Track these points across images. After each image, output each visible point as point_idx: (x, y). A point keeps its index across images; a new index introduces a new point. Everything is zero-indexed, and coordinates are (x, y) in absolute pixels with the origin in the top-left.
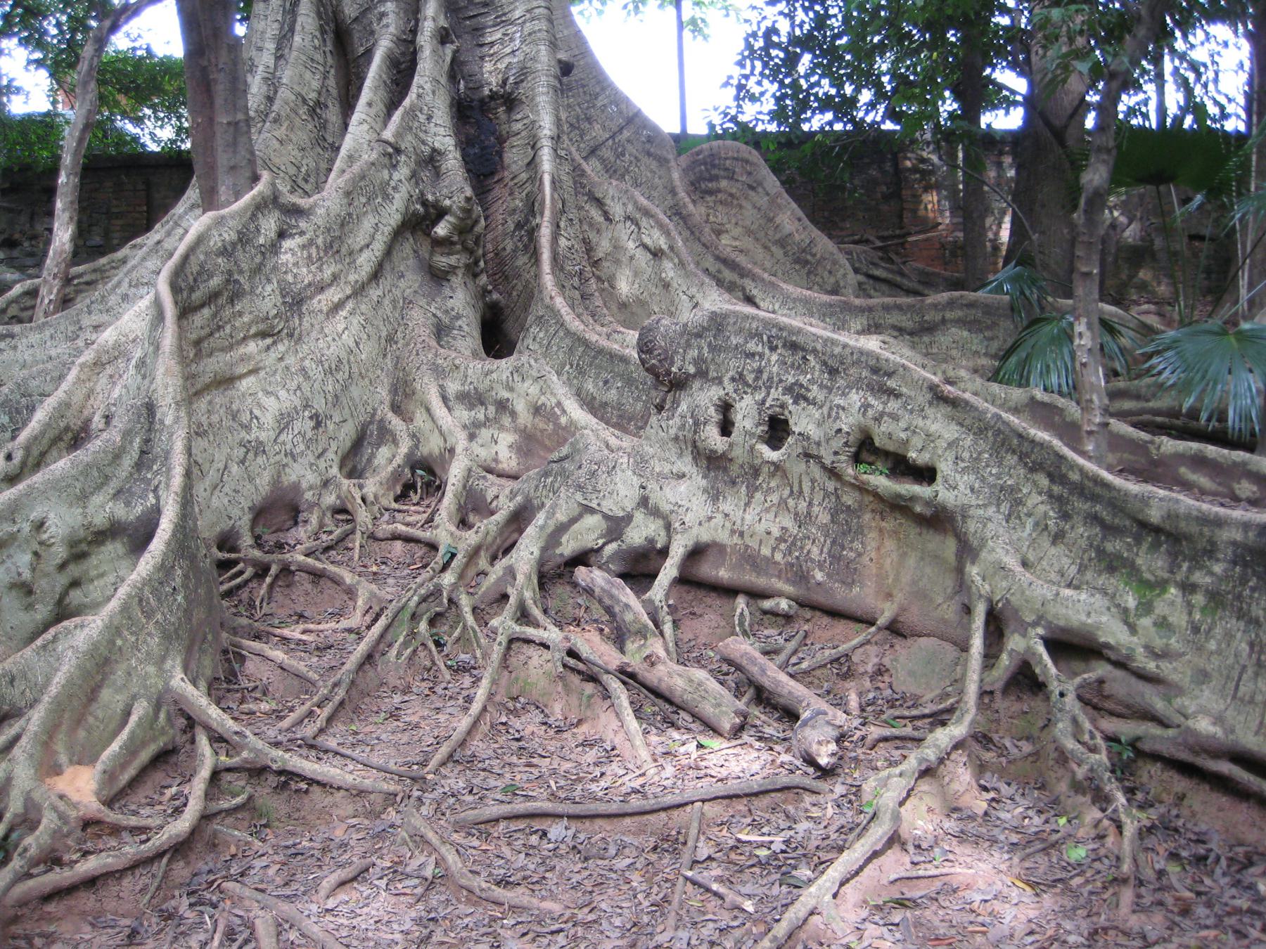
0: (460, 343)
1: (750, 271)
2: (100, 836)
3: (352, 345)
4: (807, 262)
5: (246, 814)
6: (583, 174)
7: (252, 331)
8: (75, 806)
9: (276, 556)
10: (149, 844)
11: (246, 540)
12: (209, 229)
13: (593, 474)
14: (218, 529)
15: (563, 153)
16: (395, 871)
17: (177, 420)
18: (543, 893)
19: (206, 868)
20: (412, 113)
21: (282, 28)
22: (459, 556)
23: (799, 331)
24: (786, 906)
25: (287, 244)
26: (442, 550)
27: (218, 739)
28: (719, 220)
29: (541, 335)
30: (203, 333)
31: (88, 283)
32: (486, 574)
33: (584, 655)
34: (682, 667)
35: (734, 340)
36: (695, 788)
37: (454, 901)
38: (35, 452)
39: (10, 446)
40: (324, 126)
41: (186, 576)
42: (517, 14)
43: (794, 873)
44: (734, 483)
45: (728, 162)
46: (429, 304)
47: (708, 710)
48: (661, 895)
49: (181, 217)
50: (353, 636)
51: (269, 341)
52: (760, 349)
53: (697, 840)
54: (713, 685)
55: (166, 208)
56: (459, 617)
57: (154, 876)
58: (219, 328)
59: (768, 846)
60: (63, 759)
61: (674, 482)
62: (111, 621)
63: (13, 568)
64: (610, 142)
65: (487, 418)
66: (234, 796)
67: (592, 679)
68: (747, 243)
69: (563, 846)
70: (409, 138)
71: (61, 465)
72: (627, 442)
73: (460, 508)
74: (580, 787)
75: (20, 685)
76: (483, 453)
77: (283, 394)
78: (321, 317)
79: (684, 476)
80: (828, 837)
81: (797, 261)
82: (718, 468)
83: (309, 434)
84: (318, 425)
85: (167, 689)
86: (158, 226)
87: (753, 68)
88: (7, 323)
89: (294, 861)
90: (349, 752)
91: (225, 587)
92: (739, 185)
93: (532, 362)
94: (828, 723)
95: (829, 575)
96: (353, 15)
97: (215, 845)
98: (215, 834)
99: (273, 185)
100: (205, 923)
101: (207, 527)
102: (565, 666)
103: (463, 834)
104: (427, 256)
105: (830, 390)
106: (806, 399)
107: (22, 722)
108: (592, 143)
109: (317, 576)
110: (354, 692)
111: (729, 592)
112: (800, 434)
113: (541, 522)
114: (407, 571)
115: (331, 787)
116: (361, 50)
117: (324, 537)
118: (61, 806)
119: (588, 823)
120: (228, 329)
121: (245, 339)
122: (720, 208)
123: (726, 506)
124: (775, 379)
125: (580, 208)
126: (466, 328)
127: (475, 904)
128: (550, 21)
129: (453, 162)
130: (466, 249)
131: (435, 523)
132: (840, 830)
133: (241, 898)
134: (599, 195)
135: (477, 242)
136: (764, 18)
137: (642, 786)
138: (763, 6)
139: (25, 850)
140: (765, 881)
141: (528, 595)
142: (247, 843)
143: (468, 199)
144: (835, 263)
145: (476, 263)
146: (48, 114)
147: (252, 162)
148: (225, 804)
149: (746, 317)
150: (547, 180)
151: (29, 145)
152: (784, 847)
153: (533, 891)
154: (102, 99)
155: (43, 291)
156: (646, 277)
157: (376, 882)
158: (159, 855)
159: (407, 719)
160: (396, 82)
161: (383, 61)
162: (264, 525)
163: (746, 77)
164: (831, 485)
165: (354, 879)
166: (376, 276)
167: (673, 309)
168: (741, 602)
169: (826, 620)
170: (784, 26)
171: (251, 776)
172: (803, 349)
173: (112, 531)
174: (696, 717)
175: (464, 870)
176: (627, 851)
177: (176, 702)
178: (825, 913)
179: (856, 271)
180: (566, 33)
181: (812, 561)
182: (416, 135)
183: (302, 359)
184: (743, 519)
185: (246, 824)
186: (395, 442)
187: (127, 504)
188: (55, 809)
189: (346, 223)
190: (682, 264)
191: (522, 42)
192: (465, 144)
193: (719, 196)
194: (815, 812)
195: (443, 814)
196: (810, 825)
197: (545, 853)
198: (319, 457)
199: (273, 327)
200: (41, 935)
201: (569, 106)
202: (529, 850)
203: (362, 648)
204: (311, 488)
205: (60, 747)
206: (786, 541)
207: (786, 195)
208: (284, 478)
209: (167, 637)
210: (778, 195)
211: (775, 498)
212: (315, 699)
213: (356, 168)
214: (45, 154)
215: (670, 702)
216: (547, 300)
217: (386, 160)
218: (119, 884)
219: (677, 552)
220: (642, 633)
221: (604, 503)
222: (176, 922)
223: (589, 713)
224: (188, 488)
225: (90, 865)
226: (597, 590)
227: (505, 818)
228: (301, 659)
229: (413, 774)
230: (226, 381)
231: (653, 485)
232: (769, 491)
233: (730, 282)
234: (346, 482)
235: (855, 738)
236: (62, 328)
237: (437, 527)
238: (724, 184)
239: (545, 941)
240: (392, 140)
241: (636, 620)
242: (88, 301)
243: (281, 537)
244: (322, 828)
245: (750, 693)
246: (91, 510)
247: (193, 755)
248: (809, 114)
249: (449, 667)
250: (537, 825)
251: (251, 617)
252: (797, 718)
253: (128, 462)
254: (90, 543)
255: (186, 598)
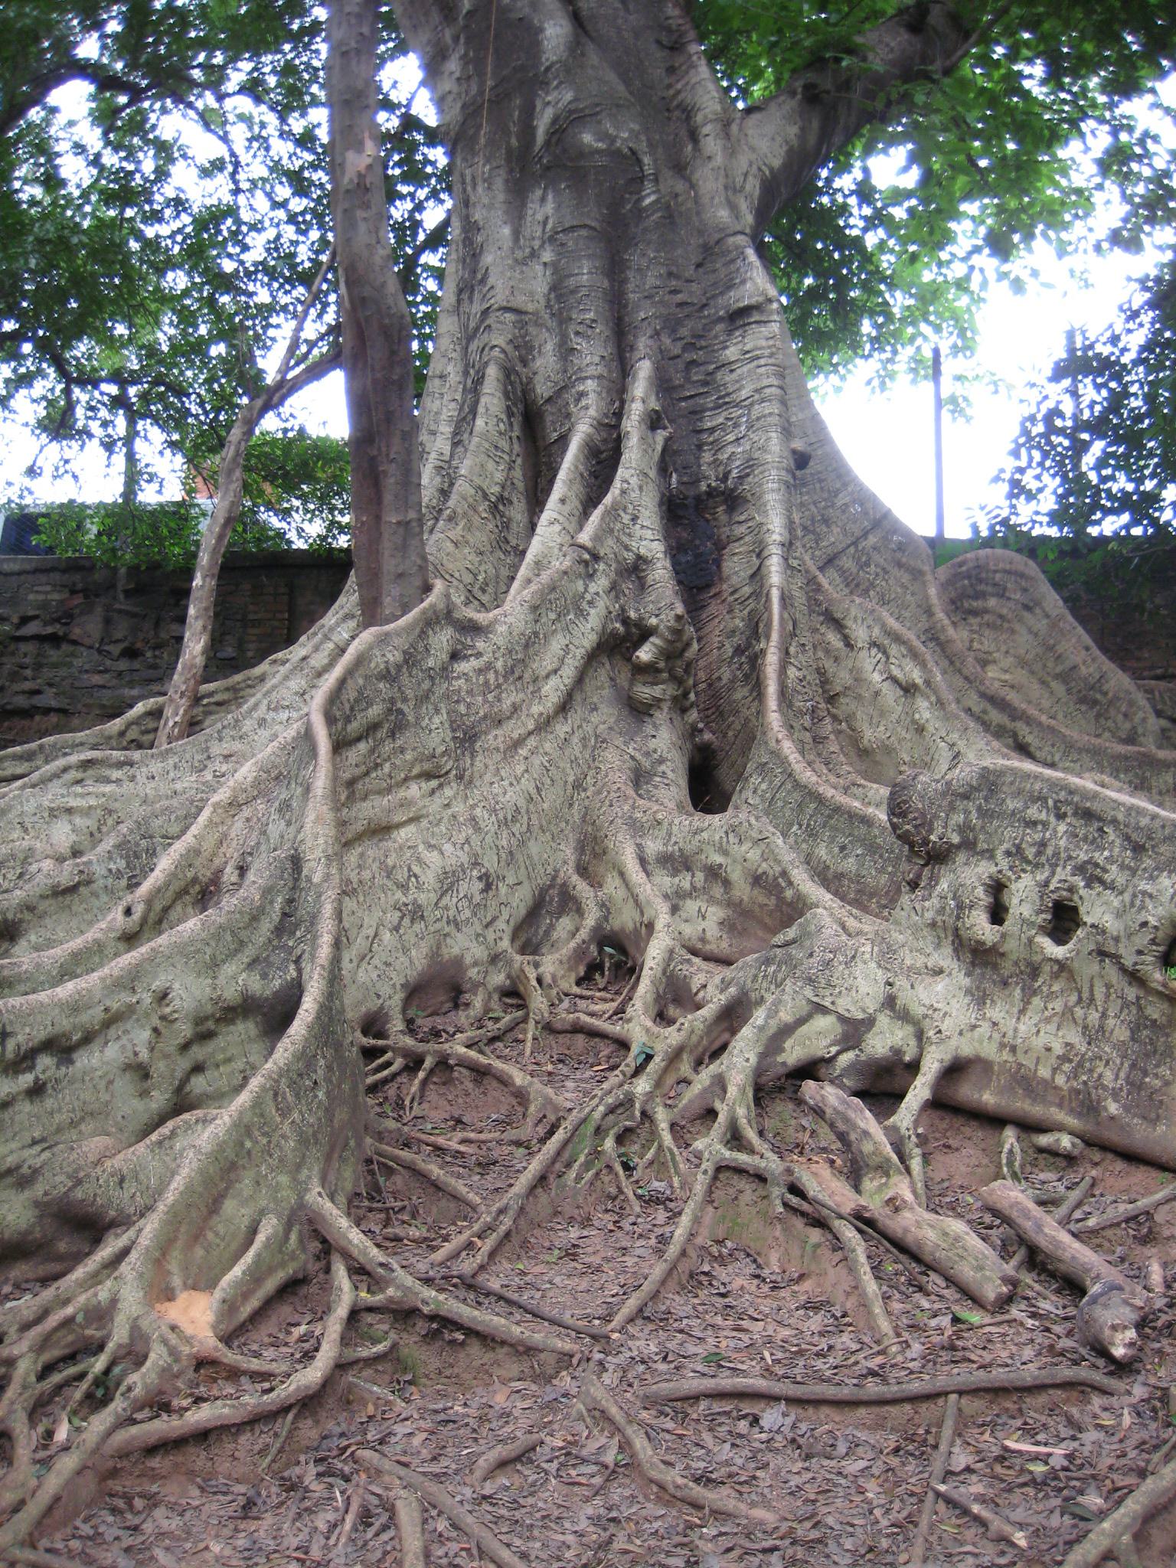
0: (662, 793)
1: (1024, 712)
2: (215, 1380)
3: (533, 791)
4: (1095, 702)
5: (388, 1366)
6: (819, 588)
7: (415, 771)
8: (188, 1340)
9: (432, 1046)
10: (273, 1395)
11: (397, 1025)
12: (371, 648)
13: (828, 964)
14: (364, 1009)
15: (795, 563)
16: (568, 1454)
17: (327, 877)
18: (754, 1497)
19: (338, 1430)
20: (613, 513)
21: (461, 409)
22: (657, 1059)
23: (1096, 796)
24: (1070, 1544)
25: (463, 667)
26: (635, 1049)
27: (359, 1271)
28: (985, 648)
29: (764, 786)
30: (358, 771)
31: (219, 704)
32: (689, 1083)
33: (811, 1194)
34: (932, 1216)
35: (1012, 804)
36: (950, 1374)
37: (641, 1499)
38: (158, 907)
39: (129, 898)
40: (507, 526)
41: (330, 1068)
42: (744, 394)
43: (1080, 1499)
44: (1005, 984)
45: (998, 576)
46: (626, 743)
47: (966, 1272)
48: (905, 1513)
49: (332, 629)
50: (522, 1151)
51: (434, 783)
52: (1043, 816)
53: (952, 1444)
54: (974, 1241)
55: (313, 618)
56: (654, 1134)
57: (276, 1435)
58: (377, 766)
59: (1045, 1459)
60: (177, 1281)
61: (929, 980)
62: (240, 1118)
63: (129, 1046)
64: (852, 550)
65: (694, 888)
66: (375, 1341)
67: (820, 1223)
68: (1020, 676)
69: (779, 1438)
70: (610, 542)
71: (191, 926)
72: (869, 925)
73: (659, 998)
74: (801, 1363)
75: (130, 1188)
76: (688, 930)
77: (448, 848)
78: (498, 757)
79: (941, 972)
80: (1124, 1455)
81: (1082, 700)
82: (985, 964)
83: (477, 898)
84: (488, 887)
85: (301, 1205)
86: (303, 638)
87: (1031, 459)
88: (125, 749)
89: (445, 1431)
90: (515, 1297)
91: (370, 1080)
92: (1011, 604)
93: (753, 821)
94: (1126, 1302)
95: (1126, 1108)
96: (546, 395)
97: (349, 1402)
98: (351, 1387)
99: (447, 596)
100: (334, 1499)
101: (354, 1005)
102: (785, 1205)
103: (653, 1412)
104: (626, 685)
105: (1134, 872)
106: (1102, 882)
107: (131, 1233)
108: (829, 551)
109: (480, 1073)
110: (522, 1222)
111: (995, 1121)
112: (1093, 926)
113: (760, 1022)
114: (589, 1074)
115: (493, 1340)
116: (555, 436)
117: (490, 1024)
118: (173, 1339)
119: (811, 1410)
120: (387, 767)
121: (406, 780)
122: (987, 632)
123: (995, 1012)
124: (1063, 855)
125: (815, 631)
126: (670, 775)
127: (667, 1504)
128: (784, 403)
129: (661, 572)
130: (675, 679)
131: (627, 1016)
132: (1140, 1446)
133: (379, 1472)
134: (838, 615)
135: (687, 671)
136: (1046, 397)
137: (881, 1366)
138: (1045, 383)
139: (129, 1389)
140: (1041, 1507)
141: (741, 1111)
142: (388, 1403)
143: (679, 618)
144: (1131, 703)
145: (685, 695)
146: (181, 504)
147: (422, 569)
148: (364, 1352)
149: (1027, 776)
150: (775, 594)
151: (160, 540)
152: (1066, 1463)
153: (741, 1493)
154: (246, 487)
155: (168, 712)
156: (894, 717)
157: (545, 1465)
158: (285, 1410)
159: (587, 1260)
160: (594, 475)
161: (580, 449)
162: (419, 1007)
163: (1021, 471)
164: (1131, 993)
165: (518, 1459)
166: (564, 708)
167: (927, 759)
168: (1010, 1137)
169: (1120, 1165)
170: (1068, 407)
171: (396, 1320)
172: (1100, 819)
173: (244, 1007)
174: (951, 1281)
175: (655, 1460)
176: (860, 1449)
177: (310, 1221)
178: (1123, 1559)
179: (1159, 714)
180: (801, 416)
181: (1105, 1088)
182: (618, 539)
183: (473, 807)
184: (1016, 1030)
185: (387, 1378)
186: (580, 912)
187: (264, 976)
188: (165, 1342)
189: (531, 643)
190: (940, 703)
191: (749, 429)
192: (675, 551)
193: (986, 617)
194: (1107, 1421)
195: (630, 1385)
196: (1101, 1435)
197: (757, 1445)
198: (487, 926)
199: (439, 767)
200: (142, 1496)
201: (802, 504)
202: (736, 1440)
203: (535, 1166)
204: (475, 964)
205: (174, 1266)
206: (1070, 1061)
207: (1070, 618)
208: (445, 951)
209: (304, 1141)
210: (1060, 618)
211: (1058, 1005)
212: (476, 1227)
213: (545, 577)
214: (177, 550)
215: (916, 1258)
216: (772, 744)
217: (581, 569)
218: (235, 1441)
219: (931, 1067)
220: (884, 1169)
221: (840, 1001)
222: (299, 1494)
223: (813, 1267)
224: (336, 961)
225: (202, 1415)
226: (829, 1111)
227: (707, 1396)
228: (459, 1176)
229: (594, 1331)
230: (381, 830)
231: (901, 982)
232: (1051, 996)
233: (999, 726)
234: (518, 958)
235: (1159, 1323)
236: (188, 756)
237: (629, 1021)
238: (992, 602)
239: (755, 1561)
240: (589, 544)
241: (877, 1152)
242: (219, 726)
243: (439, 1022)
244: (480, 1391)
245: (1021, 1255)
246: (221, 980)
247: (327, 1287)
248: (1099, 515)
249: (639, 1197)
250: (747, 1408)
251: (397, 1119)
252: (1083, 1292)
253: (266, 926)
254: (218, 1021)
255: (328, 1094)
